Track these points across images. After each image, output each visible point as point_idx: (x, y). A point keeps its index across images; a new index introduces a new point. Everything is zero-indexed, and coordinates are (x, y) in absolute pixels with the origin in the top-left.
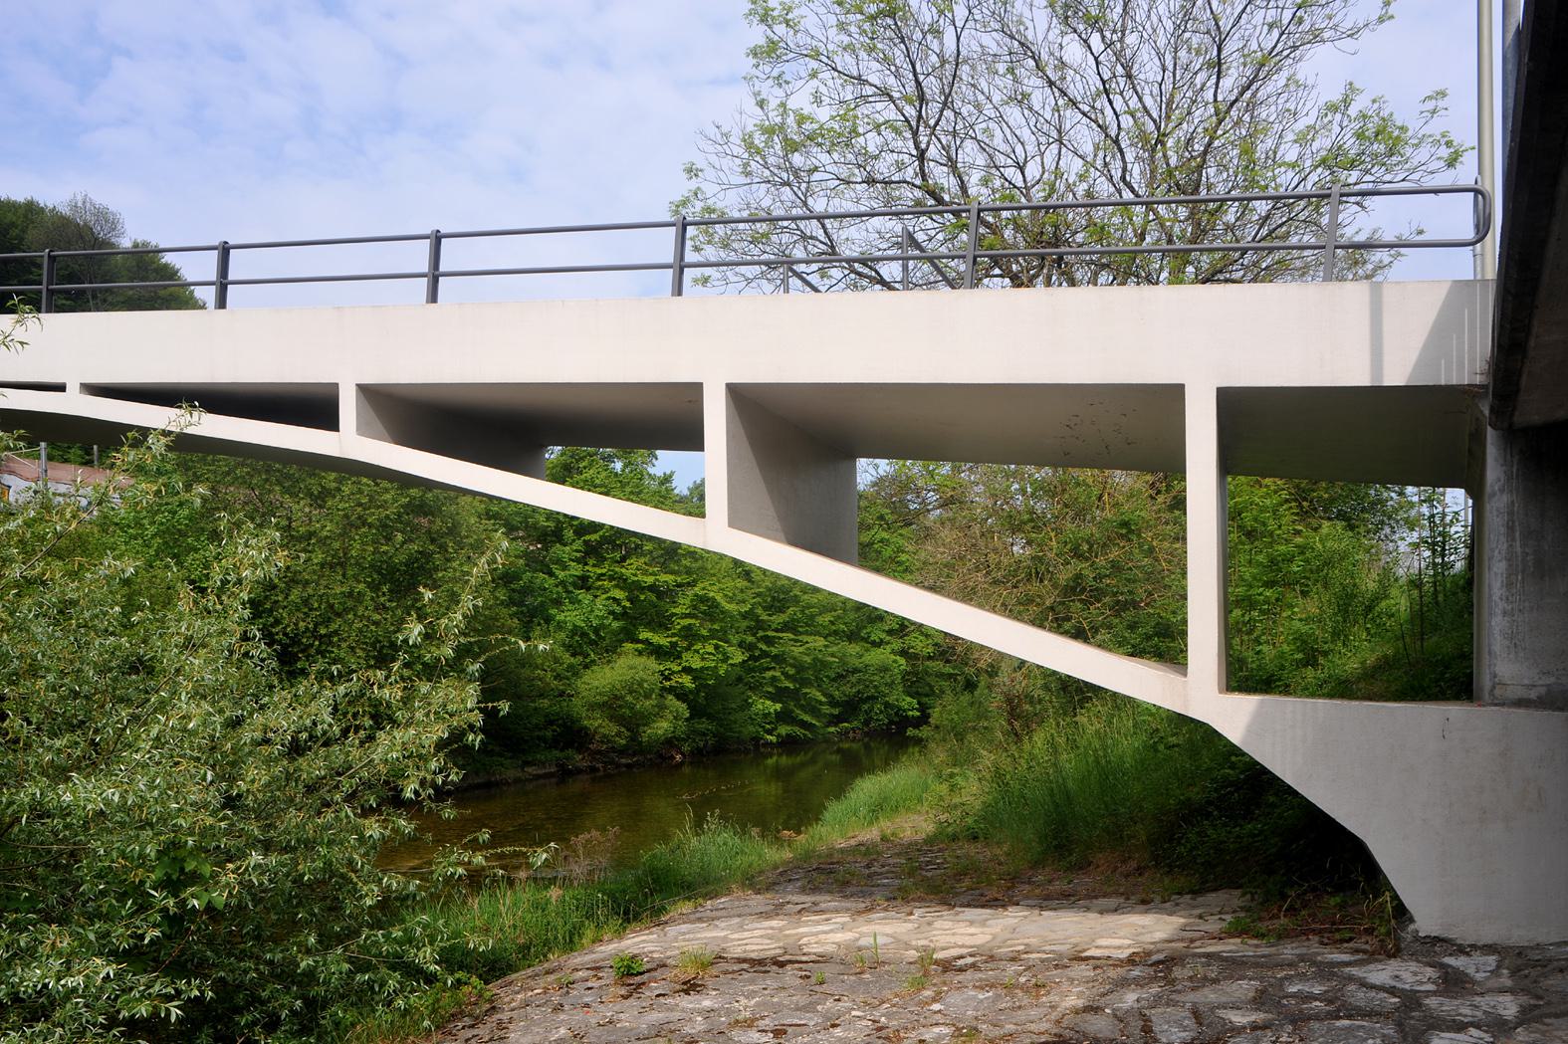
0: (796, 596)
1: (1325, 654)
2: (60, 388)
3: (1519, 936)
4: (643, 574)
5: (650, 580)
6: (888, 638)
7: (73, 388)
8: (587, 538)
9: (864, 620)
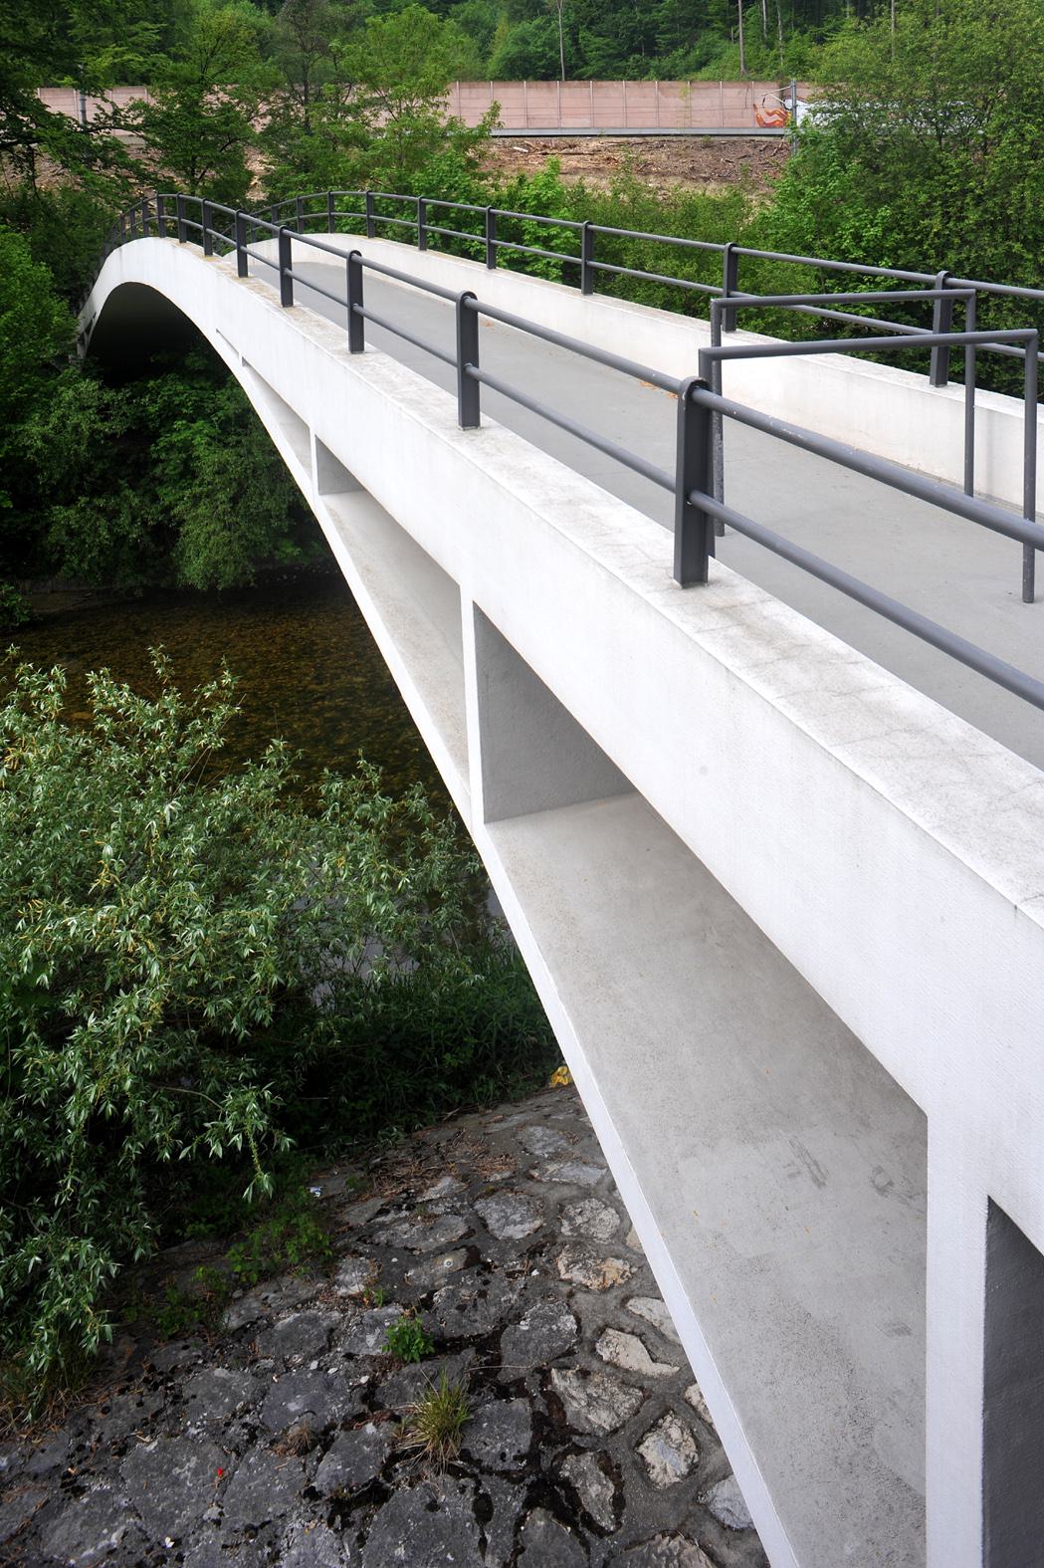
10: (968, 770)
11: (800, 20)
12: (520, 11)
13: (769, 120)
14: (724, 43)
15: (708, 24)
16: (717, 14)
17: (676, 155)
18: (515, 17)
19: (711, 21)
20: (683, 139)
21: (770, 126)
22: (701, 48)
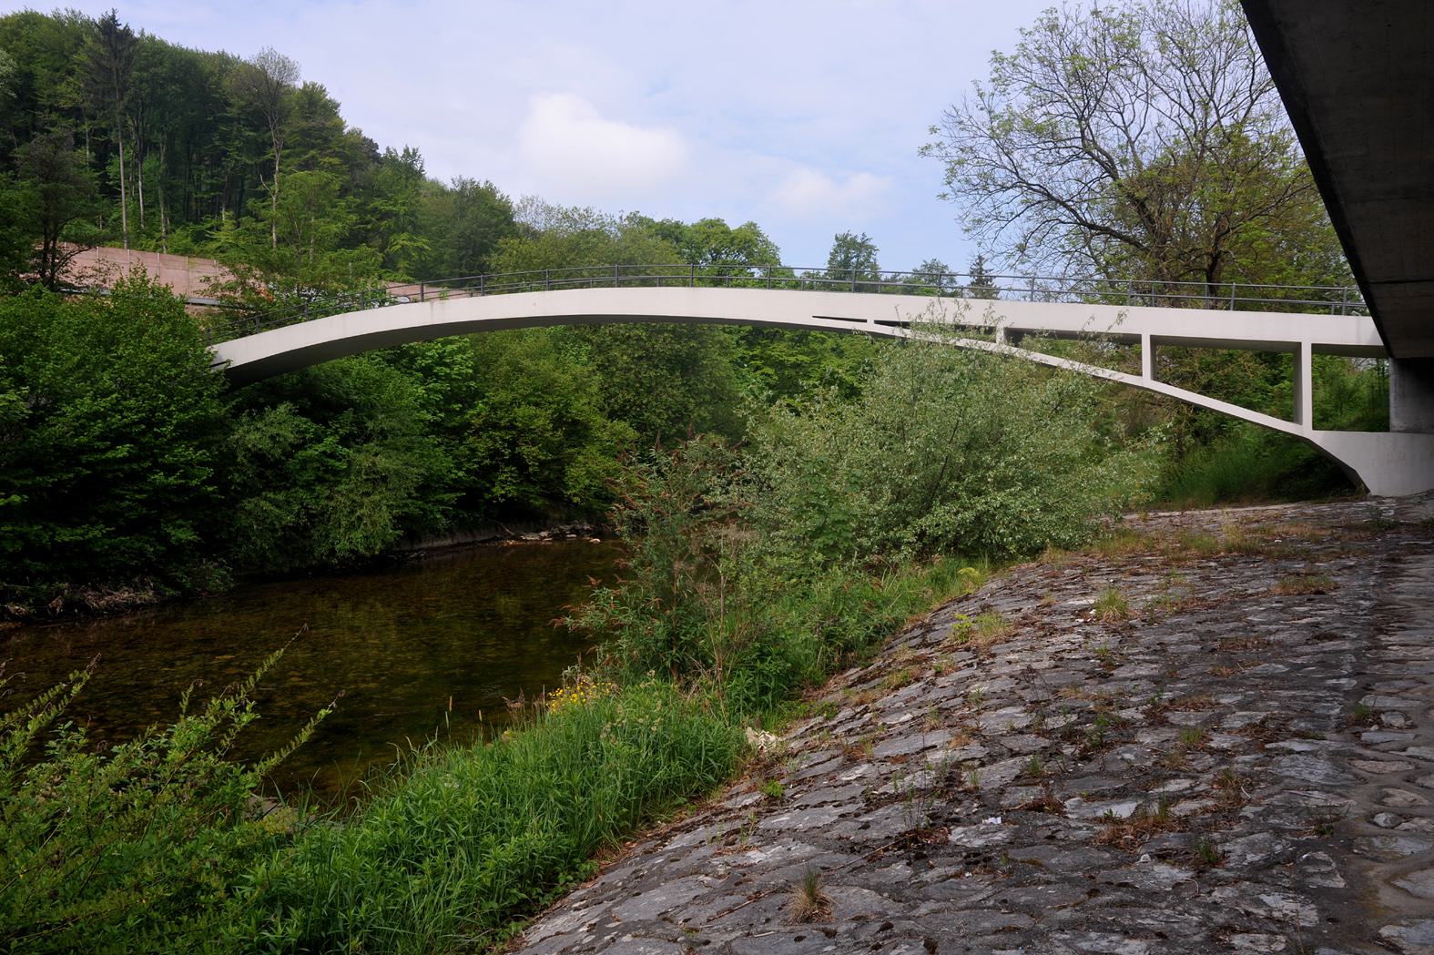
1: (1331, 416)
2: (865, 321)
3: (1399, 494)
5: (792, 359)
7: (870, 322)
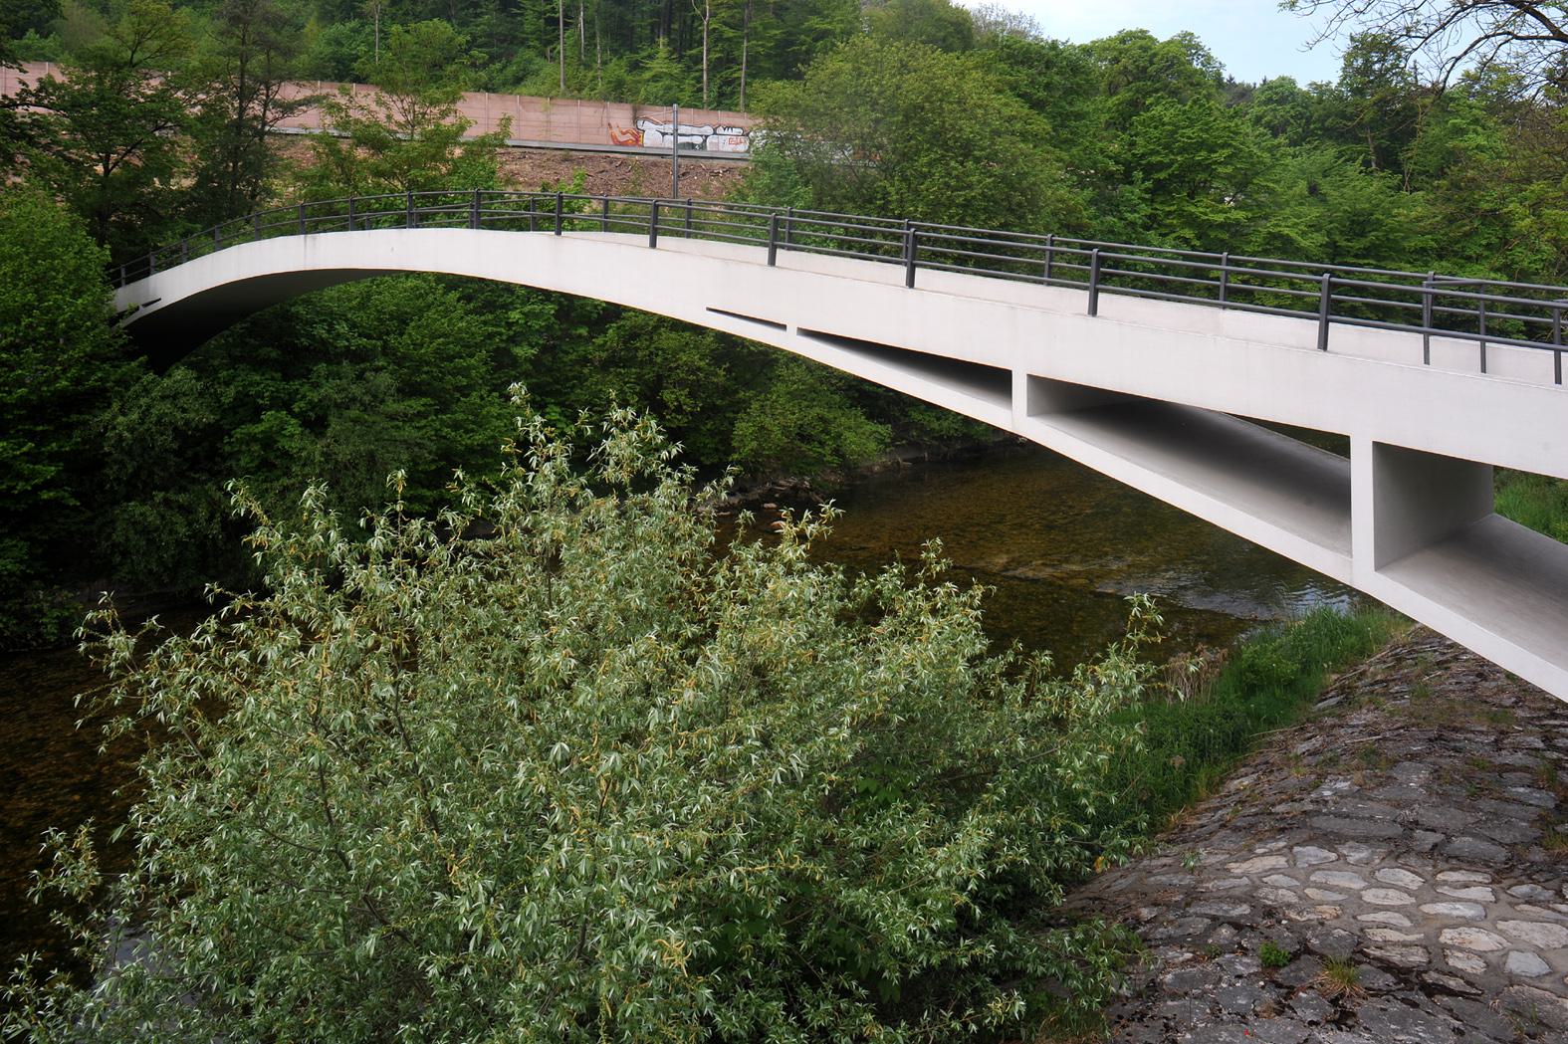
0: (1378, 219)
2: (783, 327)
4: (1212, 212)
6: (1486, 253)
7: (792, 329)
8: (1156, 176)
9: (1464, 314)
10: (1187, 782)
11: (616, 46)
12: (331, 12)
13: (622, 139)
14: (539, 60)
15: (523, 42)
16: (532, 33)
17: (539, 166)
18: (326, 17)
19: (527, 39)
20: (543, 151)
21: (622, 144)
22: (519, 63)
